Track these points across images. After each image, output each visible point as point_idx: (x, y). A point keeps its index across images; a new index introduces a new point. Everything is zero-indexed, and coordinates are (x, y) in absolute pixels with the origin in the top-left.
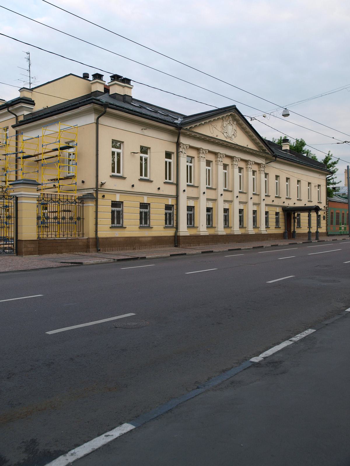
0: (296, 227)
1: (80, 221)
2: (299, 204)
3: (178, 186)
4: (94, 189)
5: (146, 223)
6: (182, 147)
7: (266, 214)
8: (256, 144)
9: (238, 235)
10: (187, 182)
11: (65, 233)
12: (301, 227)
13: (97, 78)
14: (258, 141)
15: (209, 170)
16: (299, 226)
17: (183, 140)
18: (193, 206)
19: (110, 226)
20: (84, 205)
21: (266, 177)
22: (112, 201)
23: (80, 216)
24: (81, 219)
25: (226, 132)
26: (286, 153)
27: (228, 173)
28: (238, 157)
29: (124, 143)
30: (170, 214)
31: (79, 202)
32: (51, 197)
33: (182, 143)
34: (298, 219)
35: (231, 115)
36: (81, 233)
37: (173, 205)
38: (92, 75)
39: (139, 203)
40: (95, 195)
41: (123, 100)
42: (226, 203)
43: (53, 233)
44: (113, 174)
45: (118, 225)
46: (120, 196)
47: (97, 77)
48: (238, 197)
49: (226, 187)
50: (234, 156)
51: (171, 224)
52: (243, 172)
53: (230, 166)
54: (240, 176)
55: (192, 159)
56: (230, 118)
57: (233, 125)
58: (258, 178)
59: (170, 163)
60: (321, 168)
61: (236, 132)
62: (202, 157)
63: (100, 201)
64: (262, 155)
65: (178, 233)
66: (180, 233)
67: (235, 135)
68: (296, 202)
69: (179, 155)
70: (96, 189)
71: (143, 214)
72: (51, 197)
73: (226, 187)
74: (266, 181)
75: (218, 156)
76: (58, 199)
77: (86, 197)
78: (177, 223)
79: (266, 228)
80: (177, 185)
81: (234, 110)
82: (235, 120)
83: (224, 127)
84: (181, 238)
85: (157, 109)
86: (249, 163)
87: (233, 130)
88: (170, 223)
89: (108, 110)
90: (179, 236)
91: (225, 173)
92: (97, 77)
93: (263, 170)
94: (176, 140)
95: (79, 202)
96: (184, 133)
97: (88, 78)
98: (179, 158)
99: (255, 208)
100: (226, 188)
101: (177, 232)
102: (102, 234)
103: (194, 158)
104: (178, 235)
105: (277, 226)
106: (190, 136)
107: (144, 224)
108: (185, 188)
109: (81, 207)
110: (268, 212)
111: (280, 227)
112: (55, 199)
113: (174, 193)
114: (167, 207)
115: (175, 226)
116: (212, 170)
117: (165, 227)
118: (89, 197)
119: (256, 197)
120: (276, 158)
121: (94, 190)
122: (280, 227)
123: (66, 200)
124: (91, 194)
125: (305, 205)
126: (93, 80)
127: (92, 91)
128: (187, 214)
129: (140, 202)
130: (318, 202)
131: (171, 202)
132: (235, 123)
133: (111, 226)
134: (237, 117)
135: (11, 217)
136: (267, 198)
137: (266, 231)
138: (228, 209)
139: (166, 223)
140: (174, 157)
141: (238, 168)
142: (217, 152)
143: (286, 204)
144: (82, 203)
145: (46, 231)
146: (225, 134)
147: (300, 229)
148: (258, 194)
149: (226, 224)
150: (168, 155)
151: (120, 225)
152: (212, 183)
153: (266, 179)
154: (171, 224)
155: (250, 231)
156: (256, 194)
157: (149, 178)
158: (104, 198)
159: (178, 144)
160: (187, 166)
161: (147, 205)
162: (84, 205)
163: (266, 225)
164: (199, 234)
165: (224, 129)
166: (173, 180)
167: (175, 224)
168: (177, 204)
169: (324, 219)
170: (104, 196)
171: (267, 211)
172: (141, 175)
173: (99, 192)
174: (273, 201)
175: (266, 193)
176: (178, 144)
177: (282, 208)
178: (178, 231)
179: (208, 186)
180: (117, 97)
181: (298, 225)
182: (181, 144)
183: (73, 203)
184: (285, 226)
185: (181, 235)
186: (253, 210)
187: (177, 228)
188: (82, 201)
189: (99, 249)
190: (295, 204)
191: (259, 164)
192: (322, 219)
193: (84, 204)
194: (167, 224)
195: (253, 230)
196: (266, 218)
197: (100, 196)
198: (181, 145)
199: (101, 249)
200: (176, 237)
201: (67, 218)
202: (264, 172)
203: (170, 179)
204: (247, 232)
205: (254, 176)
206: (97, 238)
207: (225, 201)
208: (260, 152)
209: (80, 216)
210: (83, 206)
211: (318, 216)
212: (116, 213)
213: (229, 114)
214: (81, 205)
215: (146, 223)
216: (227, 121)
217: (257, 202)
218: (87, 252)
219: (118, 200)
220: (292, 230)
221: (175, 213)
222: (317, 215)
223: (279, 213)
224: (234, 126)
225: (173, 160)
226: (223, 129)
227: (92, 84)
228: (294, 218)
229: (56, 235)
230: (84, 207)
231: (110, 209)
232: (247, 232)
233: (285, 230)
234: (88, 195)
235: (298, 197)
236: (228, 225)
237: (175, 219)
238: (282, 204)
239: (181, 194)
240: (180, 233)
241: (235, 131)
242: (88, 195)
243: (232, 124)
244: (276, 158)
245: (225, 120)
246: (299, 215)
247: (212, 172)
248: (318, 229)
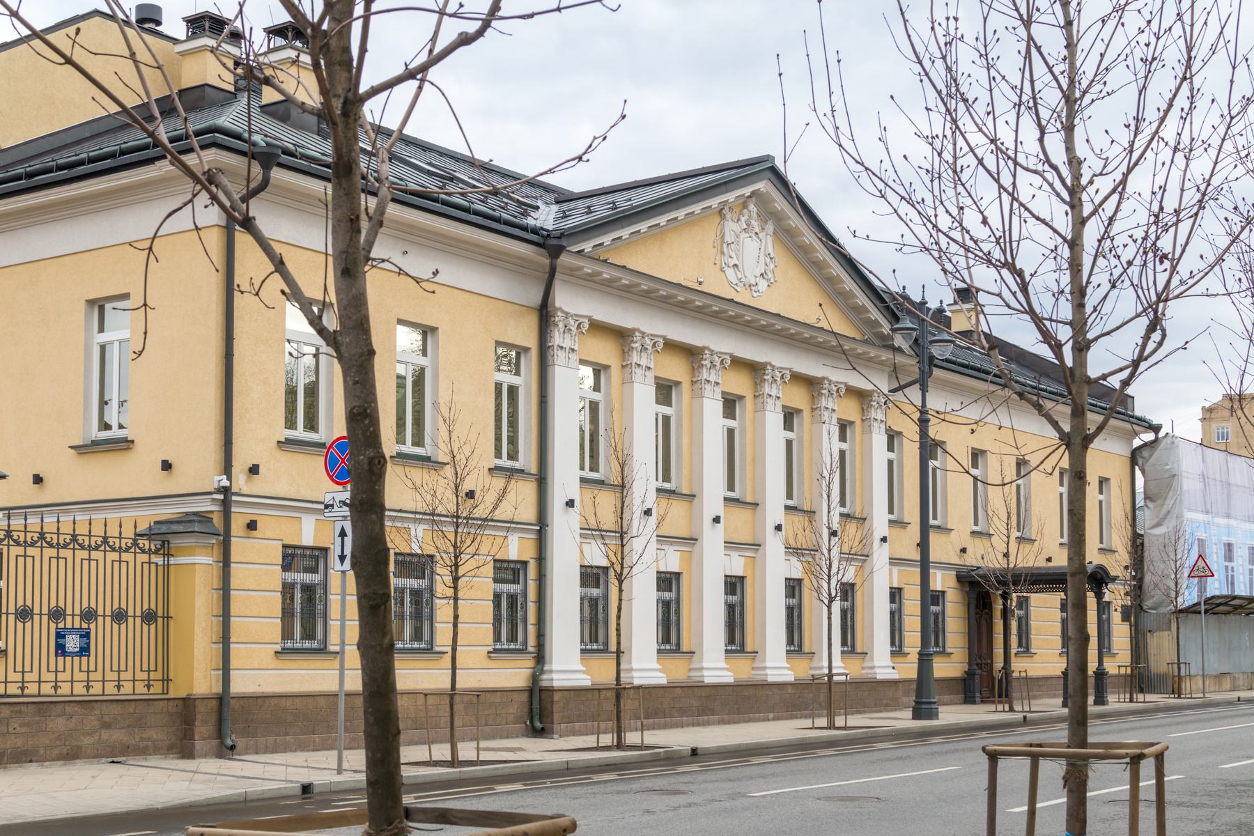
0: (1013, 651)
1: (153, 627)
2: (1027, 559)
3: (546, 483)
4: (215, 496)
5: (309, 634)
6: (561, 325)
7: (892, 600)
8: (853, 311)
9: (781, 686)
10: (582, 468)
11: (152, 676)
12: (1033, 651)
13: (208, 33)
14: (862, 299)
15: (666, 419)
16: (1025, 646)
17: (567, 300)
18: (741, 575)
19: (278, 648)
20: (172, 561)
21: (890, 448)
22: (285, 546)
23: (153, 607)
24: (160, 620)
25: (735, 265)
26: (968, 348)
27: (851, 454)
28: (723, 351)
29: (440, 330)
30: (512, 599)
31: (153, 548)
32: (9, 525)
33: (560, 309)
34: (1020, 619)
35: (753, 194)
36: (159, 675)
37: (525, 563)
38: (184, 19)
39: (280, 543)
40: (217, 521)
41: (316, 128)
42: (735, 555)
43: (140, 675)
44: (292, 434)
45: (307, 645)
46: (316, 525)
47: (207, 27)
48: (722, 520)
49: (667, 478)
50: (824, 378)
51: (421, 640)
52: (801, 424)
53: (686, 386)
54: (789, 443)
55: (425, 334)
56: (752, 207)
57: (761, 235)
58: (685, 414)
59: (513, 391)
60: (1100, 407)
61: (772, 266)
62: (639, 365)
63: (240, 547)
64: (876, 356)
65: (544, 677)
66: (555, 676)
67: (770, 275)
68: (968, 542)
69: (550, 358)
70: (221, 497)
71: (298, 596)
72: (9, 525)
73: (667, 478)
74: (890, 463)
75: (634, 345)
76: (70, 537)
77: (180, 528)
78: (541, 636)
79: (893, 653)
80: (542, 481)
81: (769, 174)
82: (768, 214)
83: (725, 245)
84: (556, 697)
85: (450, 165)
86: (823, 391)
87: (762, 255)
88: (513, 638)
89: (277, 174)
90: (551, 690)
91: (666, 419)
92: (207, 27)
93: (879, 419)
94: (535, 298)
95: (150, 550)
96: (572, 270)
97: (159, 23)
98: (550, 369)
99: (737, 565)
100: (597, 471)
101: (542, 672)
102: (241, 684)
103: (608, 371)
104: (544, 684)
105: (897, 649)
106: (591, 283)
107: (302, 639)
108: (574, 492)
109: (160, 569)
110: (900, 590)
111: (949, 650)
112: (55, 536)
113: (528, 513)
114: (588, 575)
115: (531, 649)
116: (1109, 503)
117: (283, 652)
118: (196, 529)
119: (743, 514)
120: (266, 167)
121: (214, 500)
122: (949, 650)
123: (101, 539)
124: (203, 518)
125: (1049, 560)
126: (189, 39)
127: (184, 87)
128: (582, 599)
129: (286, 542)
130: (973, 533)
131: (517, 548)
132: (770, 227)
133: (280, 650)
134: (780, 204)
135: (16, 614)
136: (897, 530)
137: (894, 668)
138: (678, 575)
139: (497, 638)
140: (530, 365)
141: (652, 381)
142: (629, 326)
143: (971, 560)
144: (162, 552)
145: (84, 668)
146: (730, 273)
147: (1029, 660)
148: (749, 500)
149: (666, 639)
150: (512, 355)
151: (315, 645)
152: (852, 502)
153: (892, 456)
154: (421, 640)
155: (879, 667)
156: (678, 491)
157: (323, 436)
158: (255, 533)
159: (545, 315)
160: (498, 387)
161: (518, 566)
162: (171, 562)
163: (893, 644)
164: (700, 679)
165: (725, 250)
166: (527, 459)
167: (532, 641)
168: (541, 558)
169: (1126, 617)
170: (252, 526)
171: (895, 585)
172: (290, 423)
173: (233, 509)
174: (964, 550)
175: (891, 511)
176: (545, 315)
177: (955, 573)
178: (546, 668)
179: (660, 484)
180: (295, 112)
181: (1020, 645)
182: (559, 314)
183: (65, 546)
184: (970, 649)
185: (556, 684)
186: (786, 579)
187: (540, 657)
188: (163, 546)
189: (229, 743)
190: (1019, 52)
191: (862, 396)
192: (1116, 617)
193: (171, 559)
194: (292, 639)
195: (724, 665)
196: (892, 613)
197: (238, 525)
198: (557, 319)
199: (241, 743)
200: (537, 692)
201: (41, 614)
202: (883, 426)
203: (513, 456)
204: (869, 671)
205: (845, 442)
206: (222, 700)
207: (730, 545)
208: (866, 342)
209: (29, 603)
210: (167, 566)
211: (1103, 607)
212: (299, 595)
213: (747, 191)
214: (159, 560)
215: (309, 634)
216: (738, 220)
217: (802, 542)
218: (187, 752)
219: (308, 539)
220: (999, 664)
221: (532, 595)
222: (1098, 603)
223: (943, 592)
224: (763, 241)
225: (526, 382)
226: (722, 253)
227: (183, 54)
228: (1006, 613)
229: (151, 683)
230: (172, 568)
231: (276, 577)
232: (869, 671)
233: (970, 664)
234: (190, 521)
235: (1101, 542)
236: (678, 644)
237: (532, 618)
238: (955, 559)
239: (637, 523)
240: (555, 676)
241: (768, 260)
242: (190, 521)
243: (757, 231)
244: (266, 167)
245: (729, 216)
246: (1023, 603)
247: (679, 425)
248: (1105, 659)
